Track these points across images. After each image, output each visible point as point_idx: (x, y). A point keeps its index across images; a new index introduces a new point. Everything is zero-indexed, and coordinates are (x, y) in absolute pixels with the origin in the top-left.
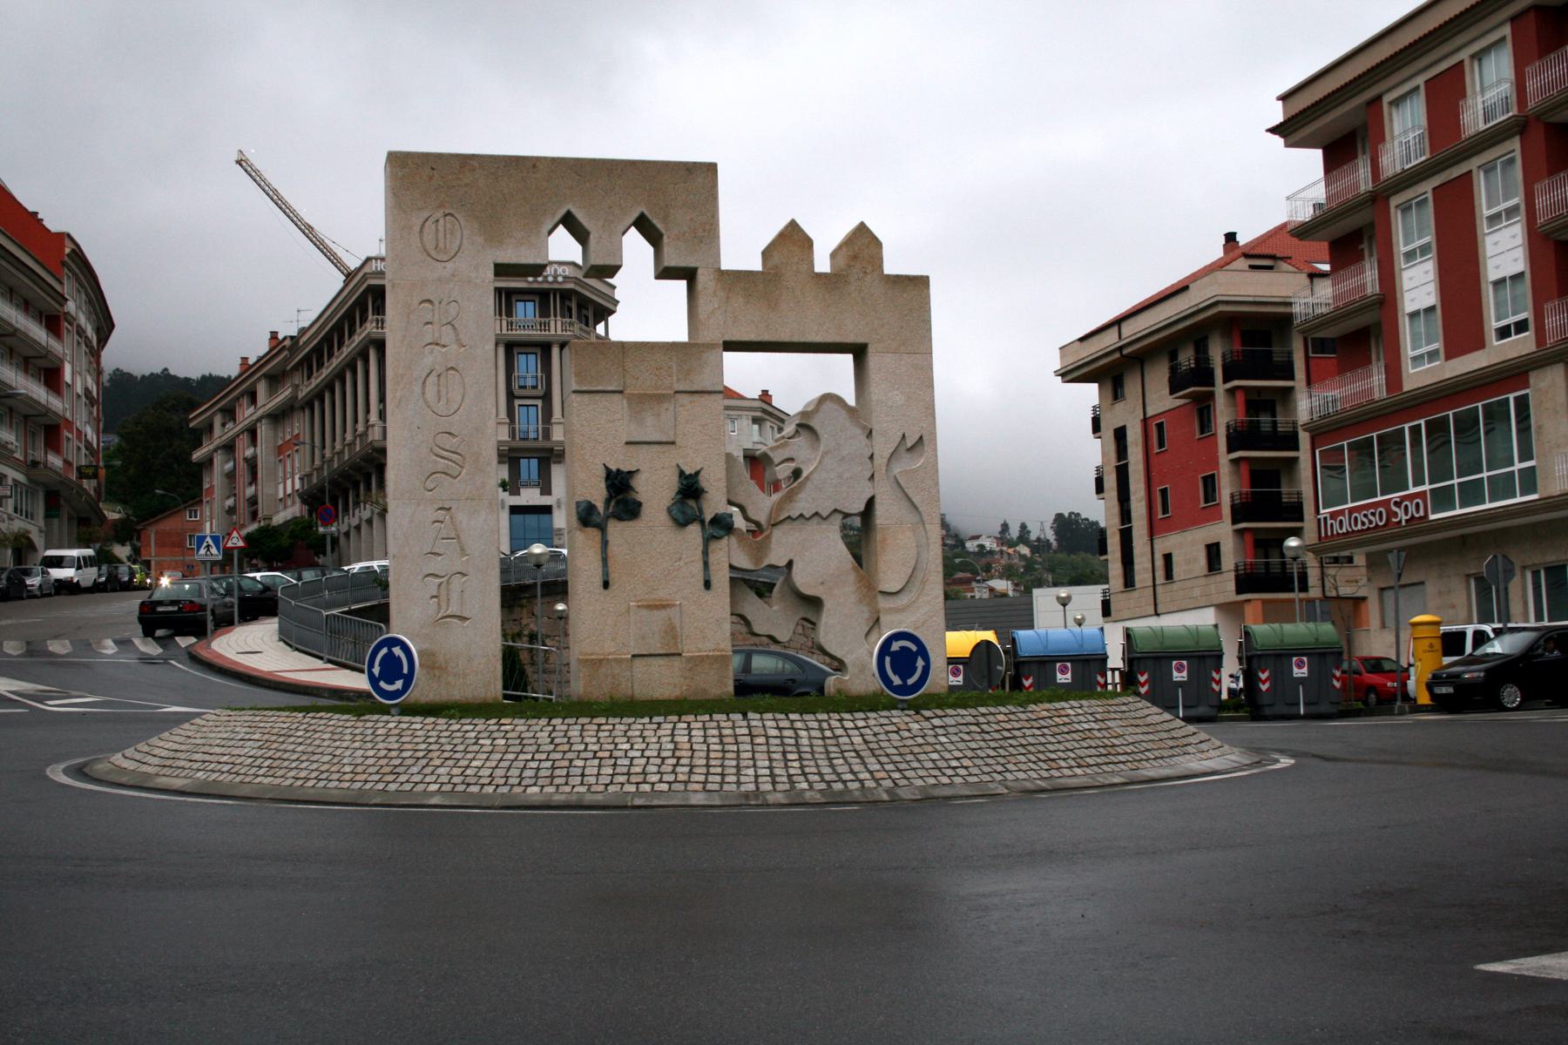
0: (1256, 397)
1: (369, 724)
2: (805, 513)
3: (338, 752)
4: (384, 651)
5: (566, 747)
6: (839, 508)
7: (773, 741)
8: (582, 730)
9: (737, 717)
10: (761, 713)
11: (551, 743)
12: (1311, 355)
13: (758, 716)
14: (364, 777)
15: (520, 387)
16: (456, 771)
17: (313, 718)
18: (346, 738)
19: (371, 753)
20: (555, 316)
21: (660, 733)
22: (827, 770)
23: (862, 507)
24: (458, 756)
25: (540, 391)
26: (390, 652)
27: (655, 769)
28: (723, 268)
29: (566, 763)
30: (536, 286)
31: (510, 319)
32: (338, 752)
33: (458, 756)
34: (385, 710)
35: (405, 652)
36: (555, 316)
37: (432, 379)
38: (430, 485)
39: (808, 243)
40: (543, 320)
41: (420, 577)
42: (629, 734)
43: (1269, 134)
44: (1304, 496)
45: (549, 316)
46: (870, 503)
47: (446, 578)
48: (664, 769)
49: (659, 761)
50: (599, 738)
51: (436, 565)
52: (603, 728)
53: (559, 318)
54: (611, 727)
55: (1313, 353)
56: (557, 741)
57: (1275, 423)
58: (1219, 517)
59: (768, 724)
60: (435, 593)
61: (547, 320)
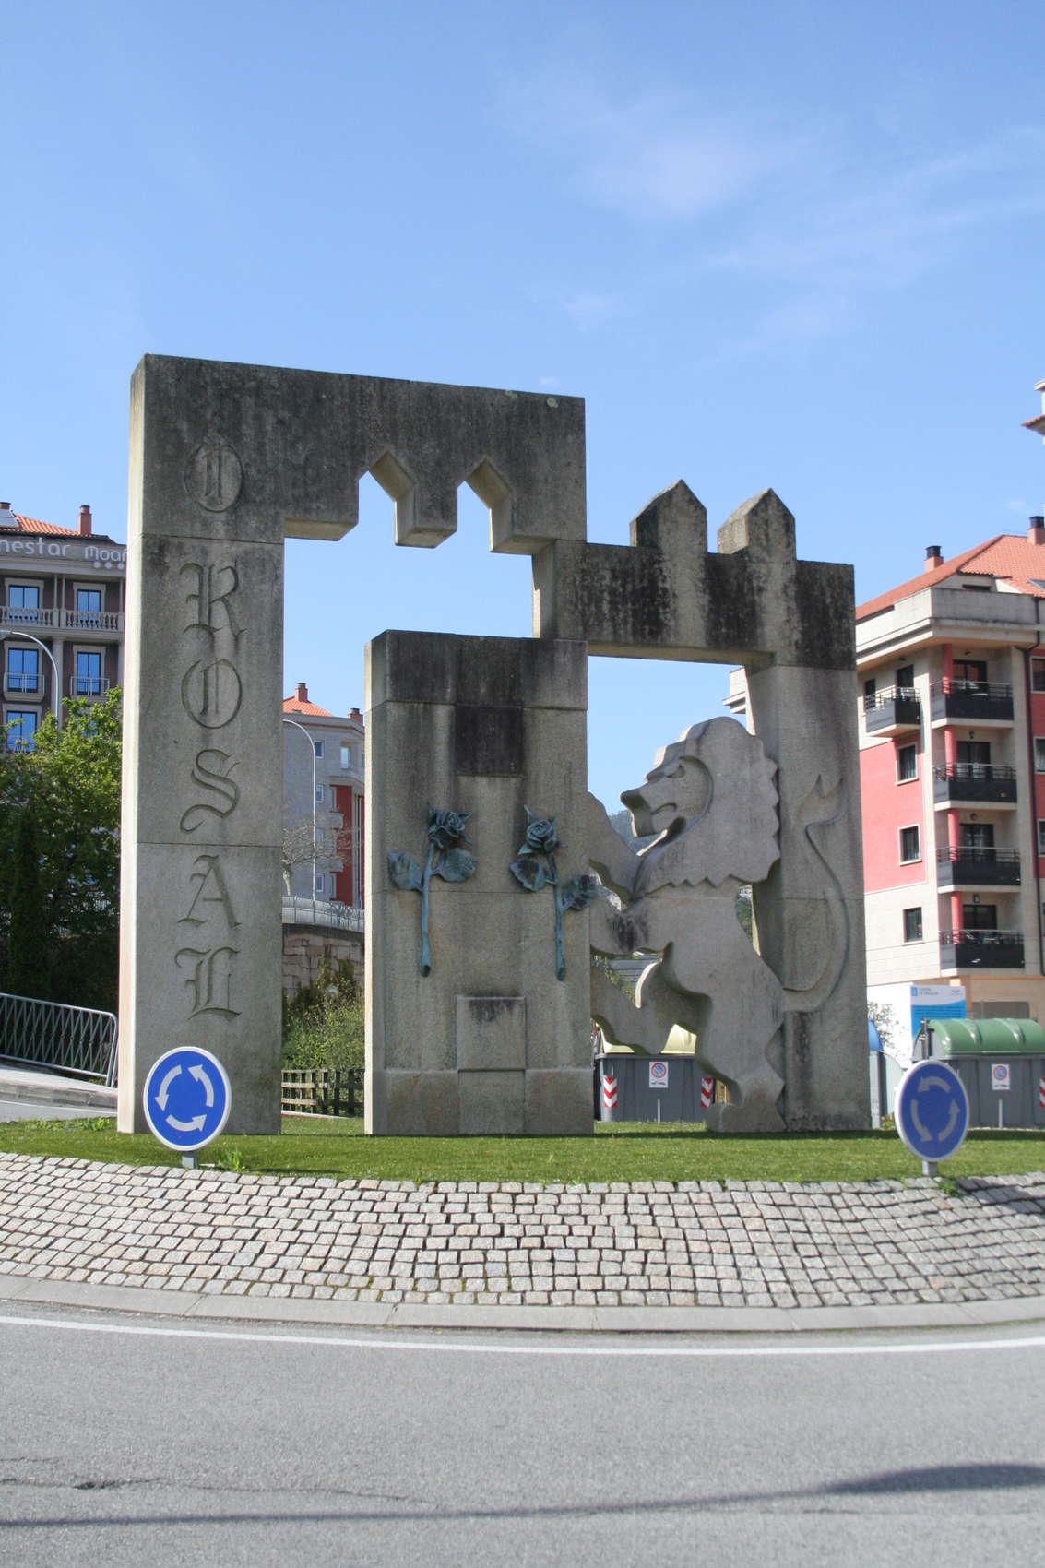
0: (968, 738)
1: (154, 1182)
2: (690, 879)
3: (113, 1224)
4: (177, 1071)
5: (473, 1229)
6: (735, 874)
7: (772, 1225)
8: (489, 1201)
9: (712, 1186)
10: (745, 1181)
11: (448, 1221)
12: (1033, 692)
13: (742, 1186)
14: (164, 1268)
15: (10, 690)
16: (310, 1264)
17: (58, 1166)
18: (120, 1201)
19: (167, 1229)
20: (59, 606)
21: (606, 1209)
22: (862, 1274)
23: (764, 874)
24: (307, 1238)
25: (38, 697)
26: (186, 1072)
27: (614, 1269)
28: (590, 540)
29: (479, 1256)
30: (104, 574)
31: (70, 612)
32: (113, 1224)
33: (307, 1238)
34: (173, 1159)
35: (211, 1077)
36: (59, 606)
37: (196, 672)
38: (189, 824)
39: (699, 510)
40: (110, 615)
41: (172, 953)
42: (561, 1209)
43: (1034, 434)
44: (1021, 856)
45: (51, 607)
46: (775, 868)
47: (209, 956)
48: (626, 1268)
49: (617, 1255)
50: (518, 1216)
51: (189, 938)
52: (519, 1199)
53: (63, 608)
54: (531, 1198)
55: (1036, 689)
56: (454, 1219)
57: (988, 771)
58: (923, 877)
59: (758, 1197)
60: (192, 977)
61: (49, 611)
